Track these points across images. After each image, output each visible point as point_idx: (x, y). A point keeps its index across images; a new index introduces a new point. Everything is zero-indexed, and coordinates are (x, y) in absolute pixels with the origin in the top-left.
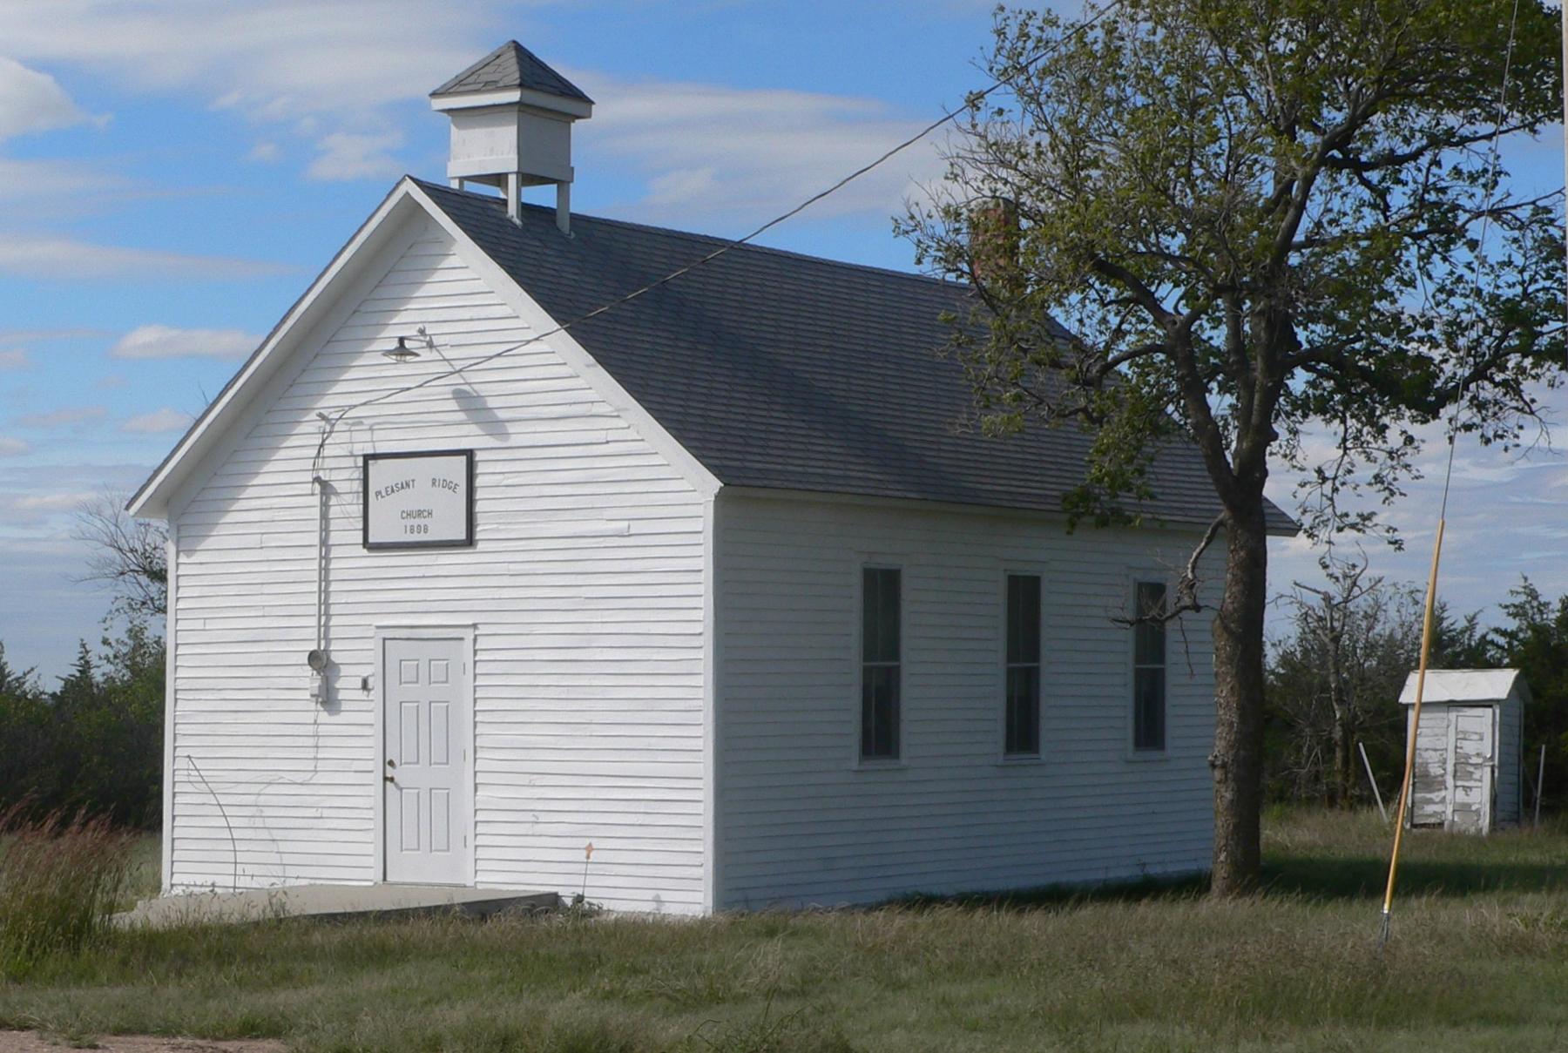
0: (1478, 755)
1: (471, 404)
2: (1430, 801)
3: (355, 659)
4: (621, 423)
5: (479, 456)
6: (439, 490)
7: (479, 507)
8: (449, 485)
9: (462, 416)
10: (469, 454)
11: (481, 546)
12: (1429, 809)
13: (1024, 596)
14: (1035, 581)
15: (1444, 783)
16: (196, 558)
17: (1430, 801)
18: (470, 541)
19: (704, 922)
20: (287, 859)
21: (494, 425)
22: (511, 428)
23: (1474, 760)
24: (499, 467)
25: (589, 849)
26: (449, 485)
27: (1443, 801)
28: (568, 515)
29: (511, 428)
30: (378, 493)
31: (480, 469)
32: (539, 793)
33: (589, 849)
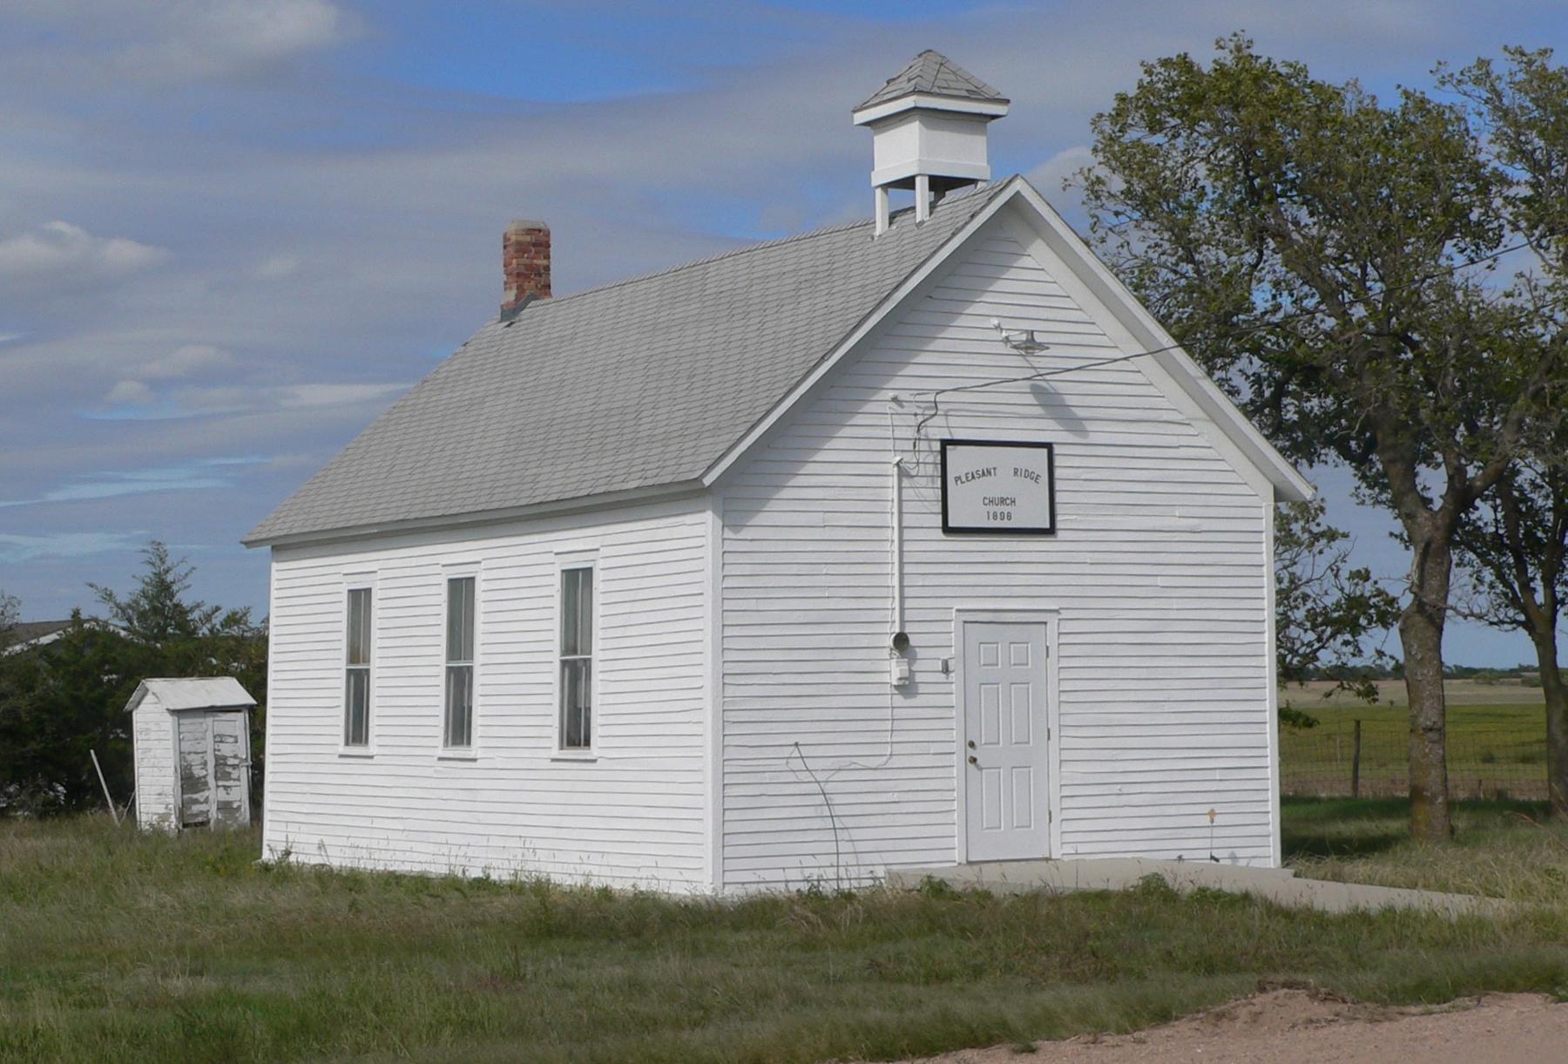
0: (235, 757)
1: (1051, 403)
2: (196, 802)
3: (938, 640)
4: (1191, 431)
5: (1057, 450)
6: (1020, 479)
7: (1059, 497)
8: (1029, 475)
9: (1039, 411)
10: (1049, 446)
11: (1060, 535)
12: (195, 808)
13: (461, 592)
14: (471, 581)
15: (206, 783)
16: (746, 533)
17: (196, 802)
18: (1051, 531)
19: (826, 898)
20: (860, 847)
21: (1073, 423)
22: (1089, 426)
23: (231, 761)
24: (1077, 462)
25: (1212, 814)
26: (1029, 475)
27: (206, 801)
28: (1144, 511)
29: (1089, 426)
30: (958, 479)
31: (1058, 461)
32: (1119, 767)
33: (1212, 814)
